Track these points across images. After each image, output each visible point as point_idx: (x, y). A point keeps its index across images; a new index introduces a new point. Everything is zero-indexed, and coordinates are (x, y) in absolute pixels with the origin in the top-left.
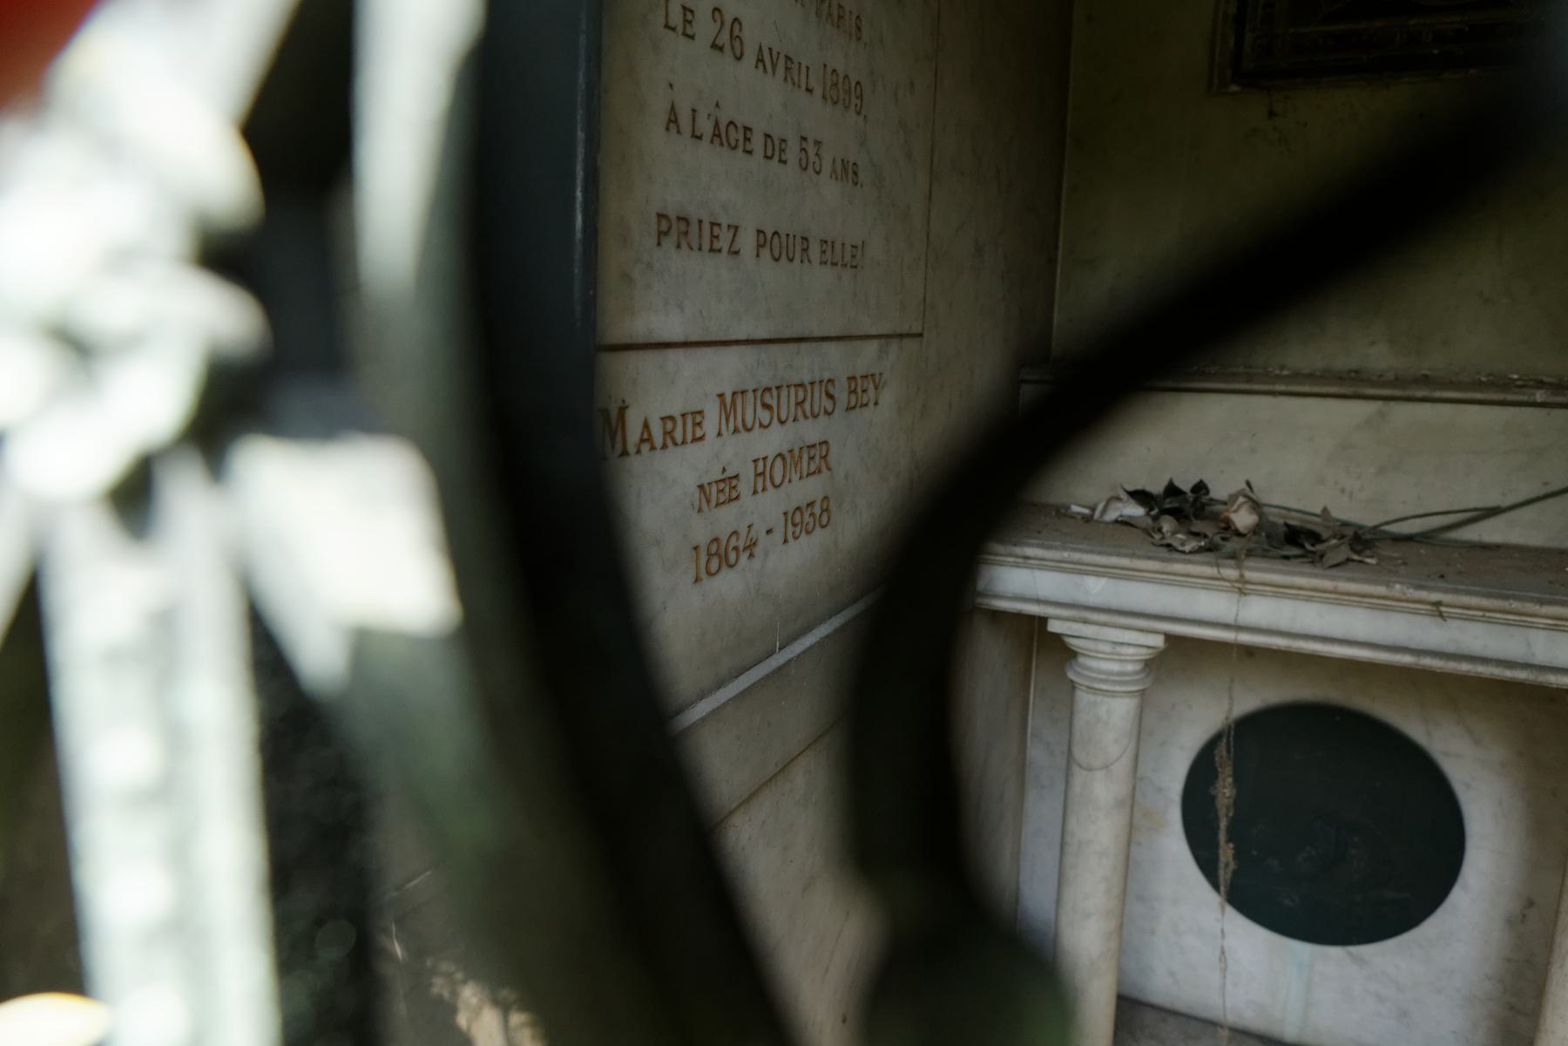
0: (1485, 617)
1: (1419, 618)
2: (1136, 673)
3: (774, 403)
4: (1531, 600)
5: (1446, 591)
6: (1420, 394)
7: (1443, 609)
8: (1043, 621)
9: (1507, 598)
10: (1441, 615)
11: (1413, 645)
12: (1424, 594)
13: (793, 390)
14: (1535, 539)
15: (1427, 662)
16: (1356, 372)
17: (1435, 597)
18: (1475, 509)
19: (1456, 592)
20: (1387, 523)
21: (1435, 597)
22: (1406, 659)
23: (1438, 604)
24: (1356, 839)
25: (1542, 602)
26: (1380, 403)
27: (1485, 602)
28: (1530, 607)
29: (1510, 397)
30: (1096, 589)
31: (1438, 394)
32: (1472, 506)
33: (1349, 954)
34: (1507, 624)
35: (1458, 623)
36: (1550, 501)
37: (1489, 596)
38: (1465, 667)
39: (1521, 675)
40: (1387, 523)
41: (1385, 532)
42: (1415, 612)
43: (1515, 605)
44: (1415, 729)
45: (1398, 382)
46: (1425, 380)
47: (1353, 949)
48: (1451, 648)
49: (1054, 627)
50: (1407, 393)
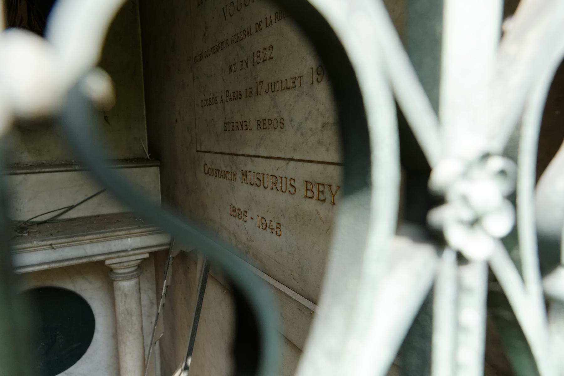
0: (69, 245)
1: (47, 251)
2: (135, 270)
3: (256, 179)
4: (81, 236)
5: (52, 240)
6: (37, 171)
7: (54, 246)
8: (103, 262)
9: (73, 237)
10: (53, 248)
11: (47, 261)
12: (45, 243)
13: (270, 177)
14: (81, 214)
15: (53, 265)
16: (18, 164)
17: (49, 242)
18: (65, 208)
19: (56, 239)
20: (33, 218)
21: (49, 242)
22: (46, 267)
23: (51, 245)
24: (58, 332)
25: (84, 236)
26: (24, 175)
27: (67, 240)
28: (81, 238)
29: (68, 169)
30: (116, 245)
31: (43, 170)
32: (66, 206)
33: (66, 373)
34: (76, 245)
35: (60, 249)
36: (89, 201)
37: (67, 238)
38: (66, 263)
39: (85, 260)
40: (33, 218)
41: (33, 222)
42: (45, 249)
43: (76, 239)
44: (70, 286)
45: (32, 166)
46: (42, 165)
47: (66, 371)
48: (61, 258)
49: (108, 262)
50: (32, 171)
